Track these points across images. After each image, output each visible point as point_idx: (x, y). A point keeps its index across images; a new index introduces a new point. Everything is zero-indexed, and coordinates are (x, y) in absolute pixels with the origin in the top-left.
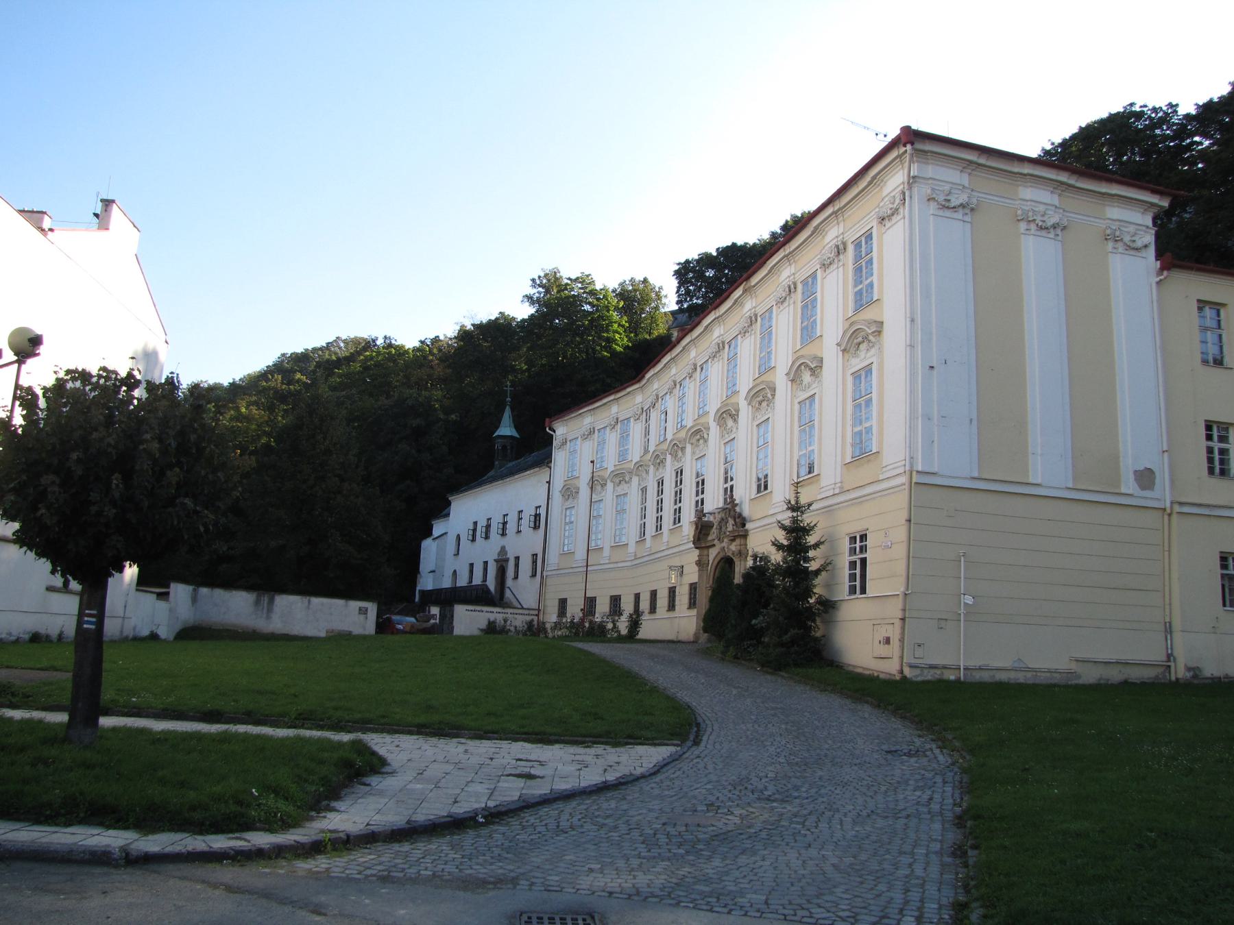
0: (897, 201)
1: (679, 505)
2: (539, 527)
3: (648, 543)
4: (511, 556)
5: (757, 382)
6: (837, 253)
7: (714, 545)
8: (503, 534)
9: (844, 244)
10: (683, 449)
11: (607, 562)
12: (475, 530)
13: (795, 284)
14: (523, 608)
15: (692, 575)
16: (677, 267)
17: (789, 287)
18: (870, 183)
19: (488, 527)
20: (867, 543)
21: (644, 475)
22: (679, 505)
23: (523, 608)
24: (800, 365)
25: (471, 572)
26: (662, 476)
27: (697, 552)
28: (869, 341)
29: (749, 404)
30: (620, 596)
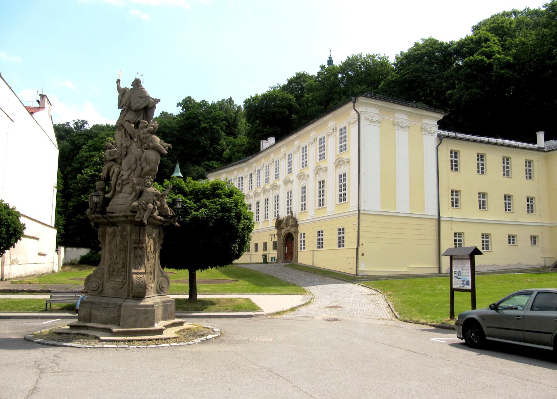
7: (284, 228)
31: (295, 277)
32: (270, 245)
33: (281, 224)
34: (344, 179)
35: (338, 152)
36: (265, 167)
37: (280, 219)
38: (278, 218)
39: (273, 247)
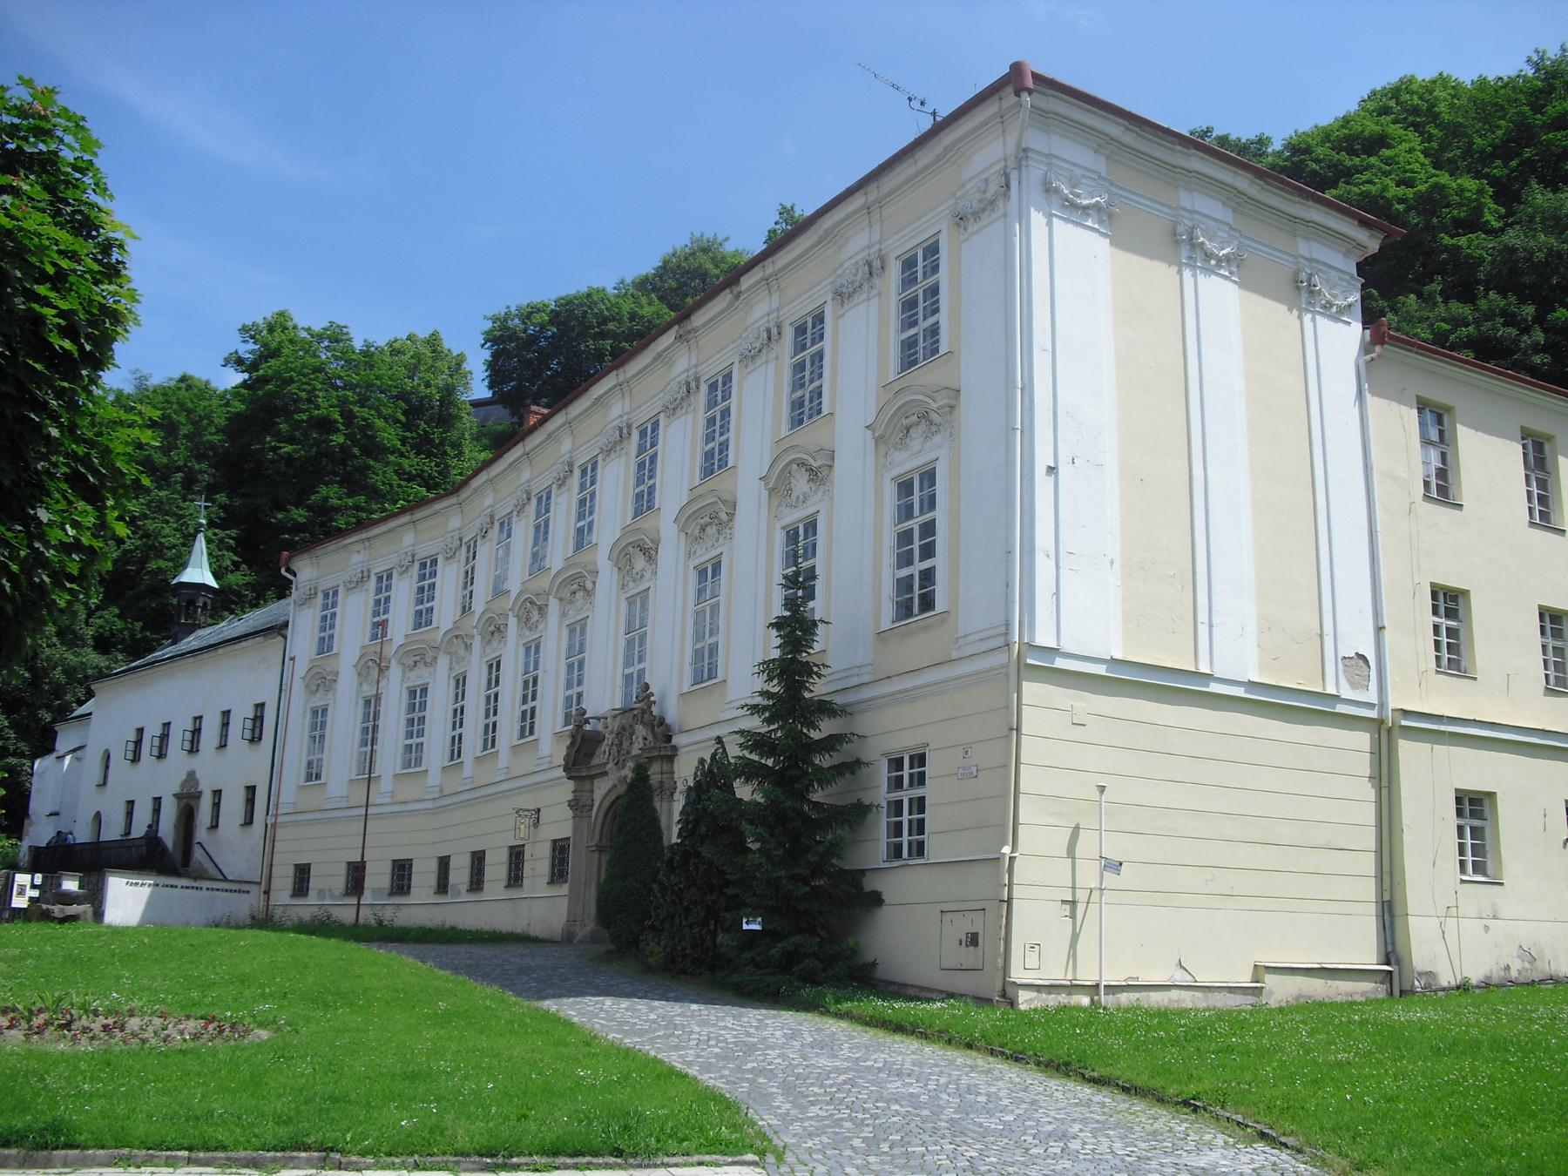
0: (993, 189)
1: (531, 704)
2: (260, 739)
3: (468, 770)
4: (206, 788)
5: (697, 492)
6: (867, 276)
7: (606, 773)
8: (193, 749)
9: (882, 259)
10: (542, 610)
11: (388, 800)
12: (138, 743)
13: (779, 327)
14: (225, 879)
15: (560, 823)
16: (488, 325)
17: (769, 331)
18: (939, 158)
19: (164, 737)
20: (926, 769)
21: (462, 652)
22: (531, 704)
23: (225, 879)
24: (791, 462)
25: (130, 814)
26: (497, 654)
27: (571, 785)
28: (931, 423)
29: (681, 530)
30: (411, 860)
31: (652, 1016)
32: (538, 864)
33: (591, 755)
34: (420, 703)
35: (784, 430)
36: (577, 473)
37: (587, 727)
38: (579, 727)
39: (553, 866)
